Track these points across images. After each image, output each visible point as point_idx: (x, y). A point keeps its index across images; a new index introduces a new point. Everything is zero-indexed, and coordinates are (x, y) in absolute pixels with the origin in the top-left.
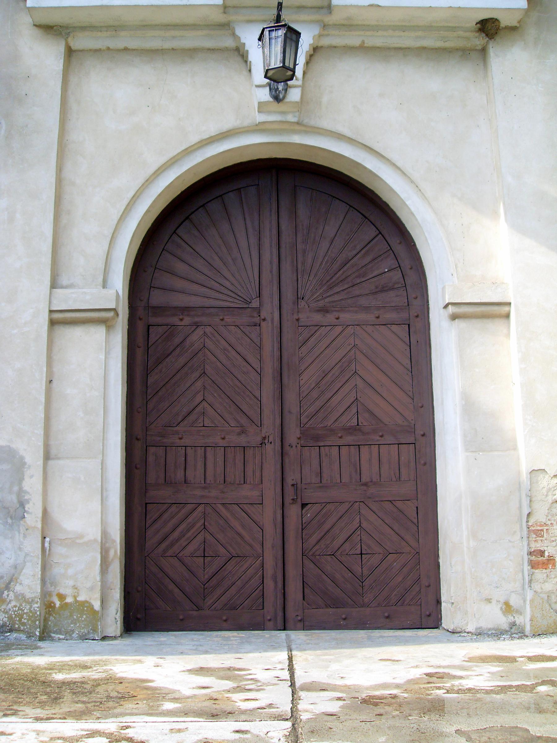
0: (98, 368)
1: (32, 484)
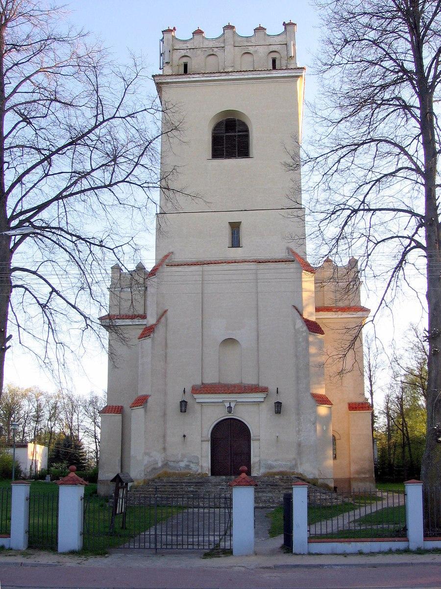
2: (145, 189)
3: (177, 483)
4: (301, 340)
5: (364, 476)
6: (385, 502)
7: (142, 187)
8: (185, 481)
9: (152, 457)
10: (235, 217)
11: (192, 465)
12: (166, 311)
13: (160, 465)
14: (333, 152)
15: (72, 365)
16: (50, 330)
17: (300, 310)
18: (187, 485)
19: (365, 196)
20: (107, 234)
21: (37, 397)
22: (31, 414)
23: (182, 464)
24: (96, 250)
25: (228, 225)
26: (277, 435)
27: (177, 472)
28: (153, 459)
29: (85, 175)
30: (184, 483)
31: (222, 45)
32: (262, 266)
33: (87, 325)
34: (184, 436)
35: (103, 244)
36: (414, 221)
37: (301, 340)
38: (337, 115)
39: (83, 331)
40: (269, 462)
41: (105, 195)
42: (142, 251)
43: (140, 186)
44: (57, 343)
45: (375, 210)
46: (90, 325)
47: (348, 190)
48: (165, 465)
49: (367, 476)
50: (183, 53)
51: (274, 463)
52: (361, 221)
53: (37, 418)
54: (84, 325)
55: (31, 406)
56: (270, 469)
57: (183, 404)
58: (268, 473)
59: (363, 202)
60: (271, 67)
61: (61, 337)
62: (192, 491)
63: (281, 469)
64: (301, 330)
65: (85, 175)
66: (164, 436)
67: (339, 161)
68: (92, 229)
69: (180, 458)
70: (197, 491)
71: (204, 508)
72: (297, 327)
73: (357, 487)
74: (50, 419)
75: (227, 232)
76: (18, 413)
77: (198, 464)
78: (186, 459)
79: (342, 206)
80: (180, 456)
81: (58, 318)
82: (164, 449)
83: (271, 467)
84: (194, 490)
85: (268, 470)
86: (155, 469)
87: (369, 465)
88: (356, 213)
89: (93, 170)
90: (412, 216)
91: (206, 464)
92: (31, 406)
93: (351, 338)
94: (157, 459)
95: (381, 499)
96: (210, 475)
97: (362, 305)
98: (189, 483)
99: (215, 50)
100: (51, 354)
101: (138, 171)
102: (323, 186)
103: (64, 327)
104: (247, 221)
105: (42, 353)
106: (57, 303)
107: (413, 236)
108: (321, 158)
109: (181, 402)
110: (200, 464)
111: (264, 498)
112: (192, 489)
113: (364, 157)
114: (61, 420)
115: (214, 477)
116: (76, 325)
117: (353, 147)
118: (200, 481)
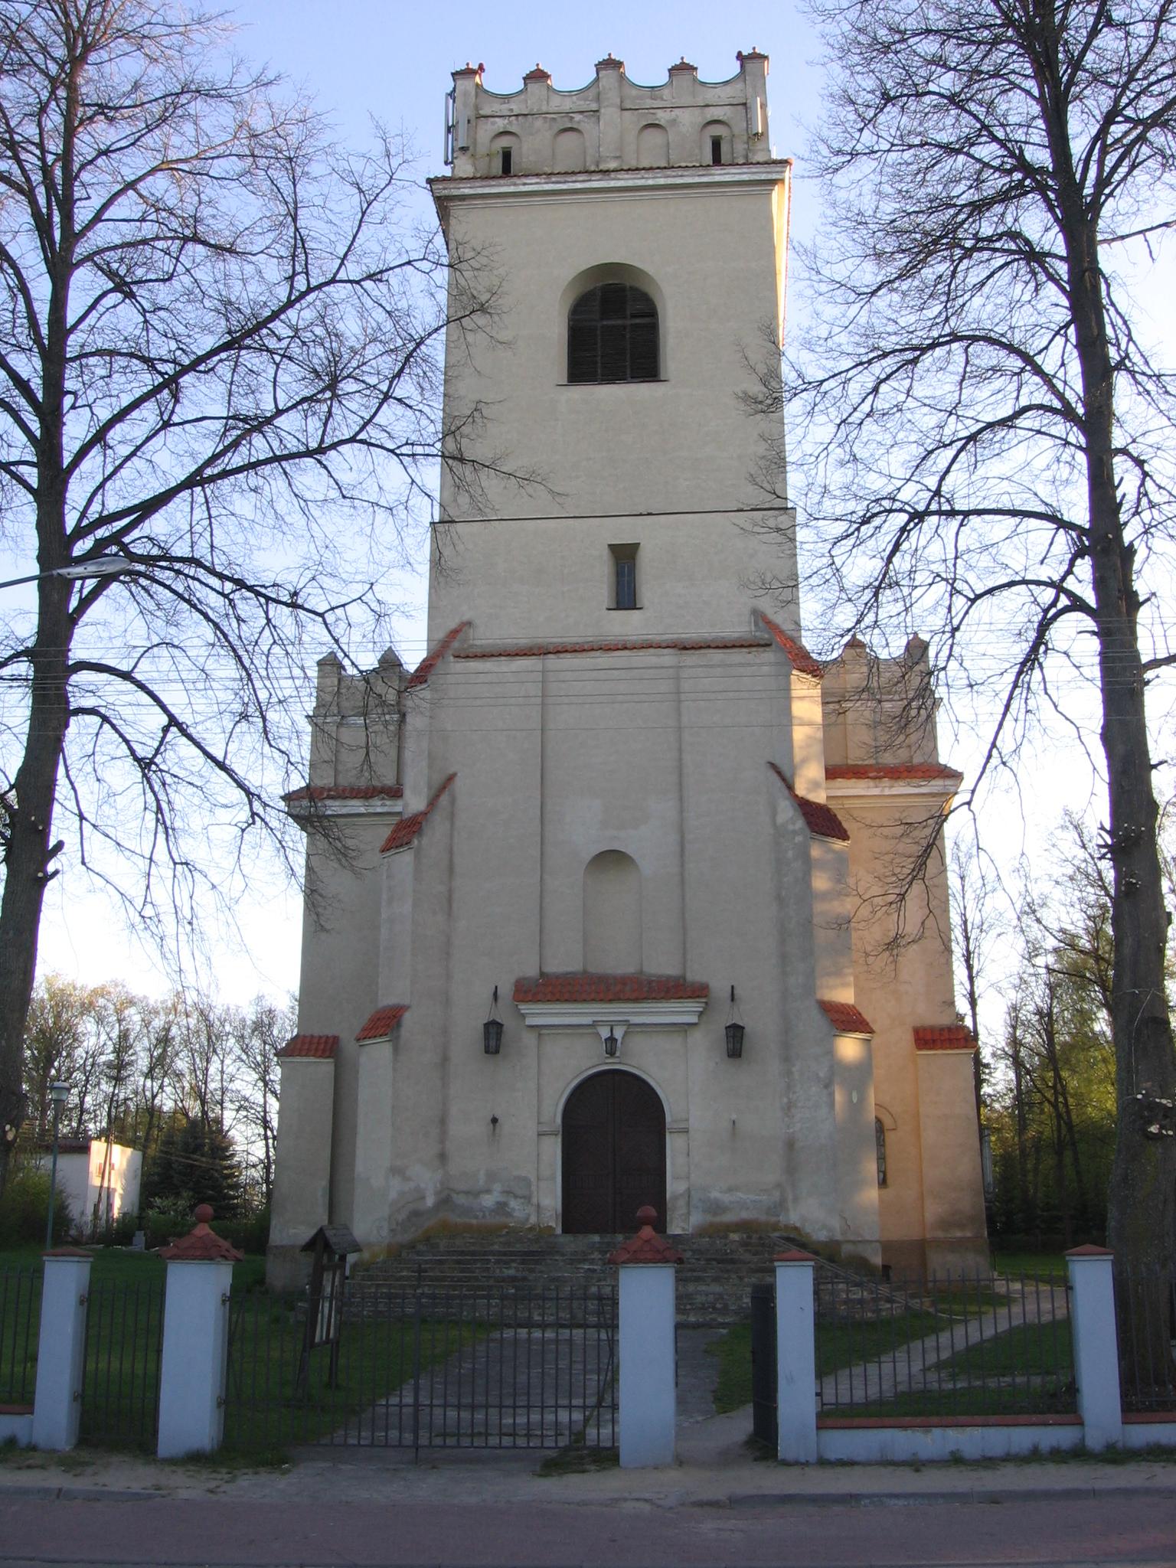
0: (553, 1149)
1: (534, 1188)
2: (406, 460)
3: (473, 1253)
4: (790, 854)
5: (959, 1234)
6: (1016, 1309)
7: (397, 455)
8: (496, 1247)
9: (409, 1179)
10: (624, 532)
11: (513, 1204)
12: (451, 778)
13: (430, 1202)
14: (860, 368)
15: (208, 924)
16: (161, 828)
17: (787, 774)
18: (498, 1262)
19: (942, 479)
20: (309, 575)
21: (119, 1011)
22: (103, 1059)
23: (488, 1201)
24: (282, 615)
25: (606, 553)
26: (734, 1117)
27: (474, 1222)
28: (412, 1185)
29: (259, 424)
30: (493, 1253)
31: (594, 106)
32: (691, 658)
33: (254, 814)
34: (494, 1121)
35: (300, 602)
36: (1063, 543)
37: (790, 854)
38: (869, 274)
39: (243, 830)
40: (715, 1194)
41: (308, 476)
42: (394, 618)
43: (392, 451)
44: (175, 864)
45: (967, 514)
46: (262, 813)
47: (898, 462)
48: (445, 1201)
49: (969, 1234)
50: (501, 124)
51: (726, 1198)
52: (934, 542)
53: (118, 1071)
54: (244, 815)
55: (103, 1037)
56: (715, 1214)
57: (493, 1030)
58: (711, 1225)
59: (937, 493)
60: (708, 158)
61: (187, 848)
62: (513, 1279)
63: (745, 1215)
64: (791, 827)
65: (259, 424)
66: (443, 1121)
67: (875, 390)
68: (272, 561)
69: (481, 1182)
70: (524, 1279)
71: (543, 1326)
72: (780, 820)
73: (944, 1265)
74: (149, 1074)
75: (603, 570)
76: (69, 1055)
77: (527, 1198)
78: (497, 1187)
79: (886, 504)
80: (482, 1175)
81: (181, 798)
82: (443, 1157)
83: (717, 1208)
84: (519, 1274)
85: (709, 1218)
86: (416, 1214)
87: (971, 1203)
88: (922, 521)
89: (279, 412)
90: (1057, 529)
91: (550, 1199)
92: (103, 1037)
93: (917, 850)
94: (422, 1185)
95: (1006, 1300)
96: (559, 1231)
97: (942, 760)
98: (505, 1254)
99: (578, 117)
100: (160, 894)
101: (389, 414)
102: (838, 453)
103: (196, 821)
104: (653, 540)
105: (137, 892)
106: (181, 755)
107: (1063, 579)
108: (832, 383)
109: (487, 1026)
110: (534, 1200)
111: (700, 1299)
112: (512, 1272)
113: (937, 378)
114: (179, 1075)
115: (569, 1238)
116: (223, 815)
117: (909, 355)
118: (533, 1248)
